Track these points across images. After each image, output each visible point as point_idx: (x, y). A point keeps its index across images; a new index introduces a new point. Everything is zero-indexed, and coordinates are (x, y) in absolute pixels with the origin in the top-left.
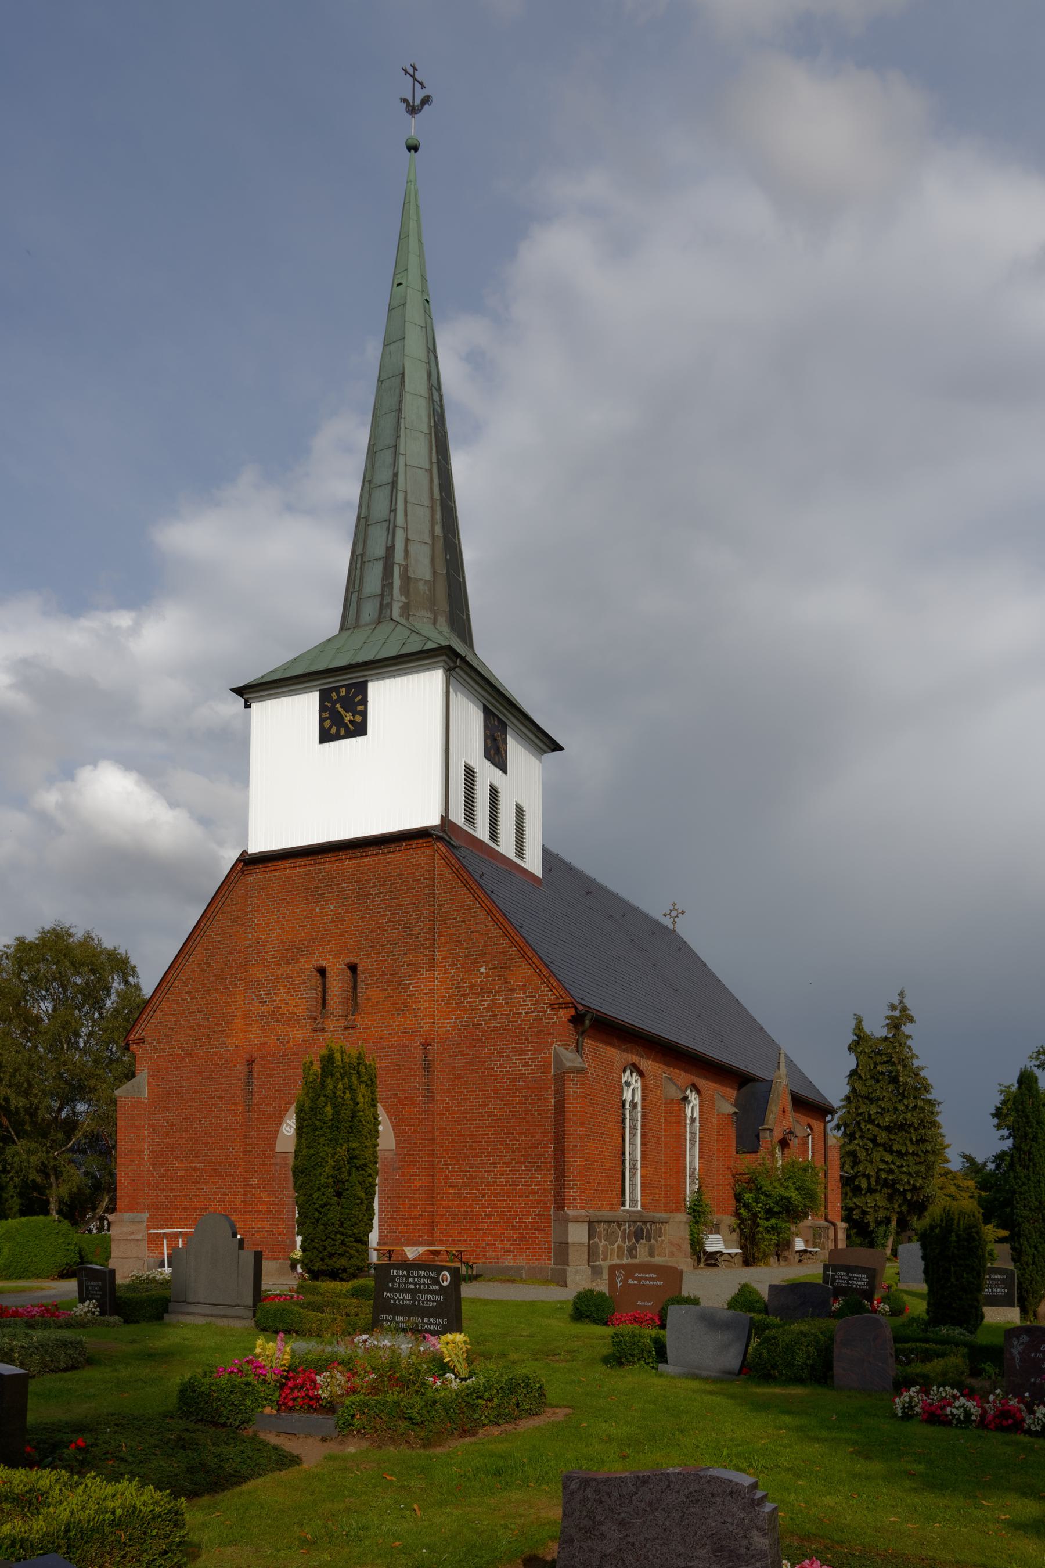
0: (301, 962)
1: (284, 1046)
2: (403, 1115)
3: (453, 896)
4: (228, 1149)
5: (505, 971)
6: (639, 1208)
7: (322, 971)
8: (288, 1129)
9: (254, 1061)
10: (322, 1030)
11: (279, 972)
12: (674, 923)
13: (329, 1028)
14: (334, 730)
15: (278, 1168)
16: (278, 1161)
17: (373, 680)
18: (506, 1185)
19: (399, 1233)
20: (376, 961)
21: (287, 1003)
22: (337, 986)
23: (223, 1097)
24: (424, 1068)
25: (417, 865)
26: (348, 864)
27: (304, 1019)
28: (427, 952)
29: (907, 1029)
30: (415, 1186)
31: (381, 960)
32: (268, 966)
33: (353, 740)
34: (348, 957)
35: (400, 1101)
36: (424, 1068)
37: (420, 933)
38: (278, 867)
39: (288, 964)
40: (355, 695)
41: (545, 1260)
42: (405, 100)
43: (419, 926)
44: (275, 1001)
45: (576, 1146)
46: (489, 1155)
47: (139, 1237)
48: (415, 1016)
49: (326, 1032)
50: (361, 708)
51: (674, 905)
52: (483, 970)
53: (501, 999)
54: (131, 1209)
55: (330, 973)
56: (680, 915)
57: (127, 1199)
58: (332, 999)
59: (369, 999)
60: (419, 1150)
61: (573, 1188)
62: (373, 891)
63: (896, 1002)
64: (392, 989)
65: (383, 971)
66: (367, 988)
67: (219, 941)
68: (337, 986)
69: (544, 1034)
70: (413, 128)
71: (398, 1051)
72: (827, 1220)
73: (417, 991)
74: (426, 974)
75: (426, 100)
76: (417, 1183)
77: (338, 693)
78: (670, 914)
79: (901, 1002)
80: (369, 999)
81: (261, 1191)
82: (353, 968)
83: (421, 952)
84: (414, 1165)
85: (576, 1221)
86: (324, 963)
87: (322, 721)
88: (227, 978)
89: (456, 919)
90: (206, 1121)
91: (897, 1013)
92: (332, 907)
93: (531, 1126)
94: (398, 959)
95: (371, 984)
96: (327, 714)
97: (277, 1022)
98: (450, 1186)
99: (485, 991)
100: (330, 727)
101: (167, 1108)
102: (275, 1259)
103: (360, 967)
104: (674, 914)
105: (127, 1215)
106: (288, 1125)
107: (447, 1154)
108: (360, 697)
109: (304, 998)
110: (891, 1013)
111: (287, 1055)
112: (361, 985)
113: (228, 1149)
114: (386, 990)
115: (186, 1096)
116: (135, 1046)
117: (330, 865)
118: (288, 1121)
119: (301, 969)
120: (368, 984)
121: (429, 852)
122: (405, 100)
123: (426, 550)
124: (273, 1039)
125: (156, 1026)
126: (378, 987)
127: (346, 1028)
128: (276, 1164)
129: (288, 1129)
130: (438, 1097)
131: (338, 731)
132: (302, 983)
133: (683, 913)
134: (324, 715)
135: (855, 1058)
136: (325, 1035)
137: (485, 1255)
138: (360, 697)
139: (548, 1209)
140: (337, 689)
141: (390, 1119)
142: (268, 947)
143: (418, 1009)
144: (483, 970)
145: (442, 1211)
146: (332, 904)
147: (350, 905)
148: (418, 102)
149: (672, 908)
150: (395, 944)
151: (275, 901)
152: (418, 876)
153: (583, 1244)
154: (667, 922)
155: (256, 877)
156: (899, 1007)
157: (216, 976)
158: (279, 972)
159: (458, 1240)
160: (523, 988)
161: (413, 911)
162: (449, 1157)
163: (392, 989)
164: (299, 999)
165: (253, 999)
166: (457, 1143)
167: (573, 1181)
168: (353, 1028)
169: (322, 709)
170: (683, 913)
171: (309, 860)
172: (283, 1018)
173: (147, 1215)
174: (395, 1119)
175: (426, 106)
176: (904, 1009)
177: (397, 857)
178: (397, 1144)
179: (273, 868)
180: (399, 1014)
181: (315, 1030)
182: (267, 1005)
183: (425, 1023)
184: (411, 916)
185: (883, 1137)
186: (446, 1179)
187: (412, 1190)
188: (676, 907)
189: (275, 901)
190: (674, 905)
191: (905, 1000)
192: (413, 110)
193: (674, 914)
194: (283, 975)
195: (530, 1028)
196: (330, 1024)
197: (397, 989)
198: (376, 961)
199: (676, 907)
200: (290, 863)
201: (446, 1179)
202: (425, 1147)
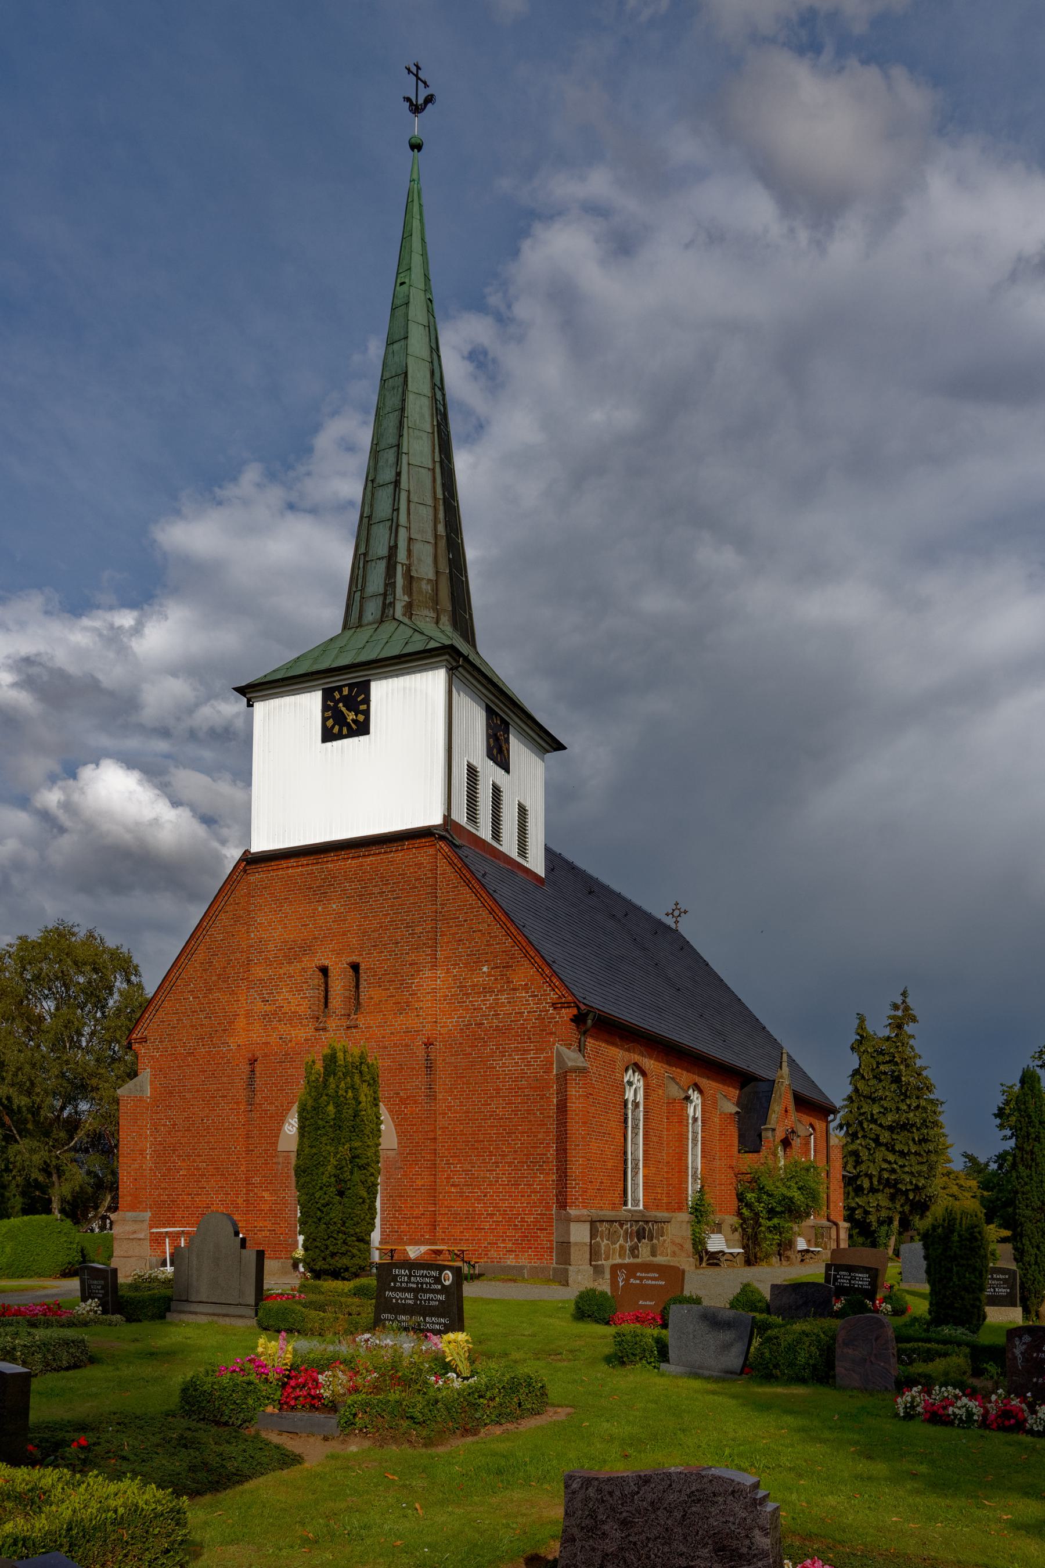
0: (303, 961)
1: (287, 1045)
2: (405, 1114)
3: (455, 895)
4: (231, 1148)
5: (507, 971)
6: (641, 1207)
7: (324, 971)
8: (290, 1128)
9: (256, 1060)
10: (324, 1029)
11: (281, 971)
12: (676, 922)
13: (331, 1027)
14: (336, 729)
15: (280, 1167)
16: (281, 1160)
17: (375, 680)
18: (508, 1185)
19: (401, 1232)
20: (378, 961)
21: (290, 1002)
22: (339, 986)
23: (226, 1096)
24: (427, 1067)
25: (419, 865)
26: (351, 863)
27: (307, 1018)
28: (429, 951)
29: (909, 1028)
30: (418, 1185)
31: (383, 960)
32: (270, 965)
33: (356, 739)
34: (351, 956)
35: (403, 1101)
36: (427, 1067)
37: (422, 933)
38: (280, 867)
39: (290, 963)
40: (358, 695)
41: (546, 1259)
42: (408, 99)
43: (422, 925)
44: (278, 1000)
45: (579, 1145)
46: (491, 1154)
47: (142, 1236)
48: (418, 1016)
49: (328, 1031)
50: (363, 707)
51: (677, 904)
52: (485, 969)
53: (503, 998)
54: (133, 1208)
55: (333, 973)
56: (682, 914)
57: (129, 1198)
58: (335, 998)
59: (372, 998)
60: (421, 1150)
61: (575, 1188)
62: (376, 890)
63: (899, 1002)
64: (395, 989)
65: (385, 970)
66: (370, 987)
67: (221, 940)
68: (339, 986)
69: (547, 1034)
70: (416, 126)
71: (400, 1050)
72: (829, 1220)
73: (419, 990)
74: (428, 974)
75: (429, 99)
76: (419, 1182)
77: (341, 692)
78: (672, 914)
79: (904, 1002)
80: (372, 998)
81: (263, 1190)
82: (355, 967)
83: (423, 952)
84: (416, 1164)
85: (579, 1220)
86: (326, 963)
87: (324, 720)
88: (229, 978)
89: (458, 918)
90: (208, 1120)
91: (899, 1013)
92: (334, 906)
93: (533, 1125)
94: (401, 958)
95: (373, 983)
96: (329, 713)
97: (280, 1021)
98: (452, 1185)
99: (487, 990)
100: (333, 727)
101: (170, 1107)
102: (276, 1258)
103: (363, 966)
104: (676, 913)
105: (130, 1214)
106: (290, 1124)
107: (450, 1153)
108: (363, 696)
109: (307, 997)
110: (893, 1013)
111: (289, 1054)
112: (363, 984)
113: (231, 1148)
114: (389, 989)
115: (188, 1096)
116: (137, 1045)
117: (333, 864)
118: (290, 1120)
119: (303, 968)
120: (370, 984)
121: (431, 851)
122: (408, 99)
123: (430, 549)
124: (276, 1038)
125: (158, 1025)
126: (380, 986)
127: (348, 1028)
128: (279, 1163)
129: (290, 1128)
130: (440, 1096)
131: (341, 730)
132: (304, 983)
133: (685, 912)
134: (326, 714)
135: (857, 1058)
136: (327, 1034)
137: (487, 1254)
138: (363, 696)
139: (549, 1208)
140: (339, 689)
141: (393, 1119)
142: (271, 947)
143: (420, 1008)
144: (485, 969)
145: (443, 1210)
146: (334, 903)
147: (352, 904)
148: (421, 101)
149: (674, 907)
150: (397, 943)
151: (278, 900)
152: (420, 875)
153: (585, 1244)
154: (669, 921)
155: (258, 876)
156: (902, 1007)
157: (219, 975)
158: (281, 971)
159: (460, 1240)
160: (526, 988)
161: (416, 911)
162: (451, 1157)
163: (395, 989)
164: (302, 998)
165: (255, 998)
166: (459, 1142)
167: (575, 1180)
168: (356, 1027)
169: (325, 708)
170: (685, 912)
171: (311, 859)
172: (285, 1017)
173: (149, 1214)
174: (398, 1118)
175: (430, 105)
176: (907, 1009)
177: (398, 856)
178: (399, 1143)
179: (275, 867)
180: (402, 1014)
181: (317, 1030)
182: (270, 1005)
183: (427, 1023)
184: (413, 915)
185: (885, 1137)
186: (448, 1178)
187: (413, 1189)
188: (678, 907)
189: (278, 900)
190: (677, 904)
191: (907, 1000)
192: (416, 109)
193: (676, 913)
194: (285, 974)
195: (532, 1027)
196: (332, 1024)
197: (400, 988)
198: (378, 961)
199: (678, 907)
200: (292, 862)
201: (448, 1178)
202: (427, 1146)
